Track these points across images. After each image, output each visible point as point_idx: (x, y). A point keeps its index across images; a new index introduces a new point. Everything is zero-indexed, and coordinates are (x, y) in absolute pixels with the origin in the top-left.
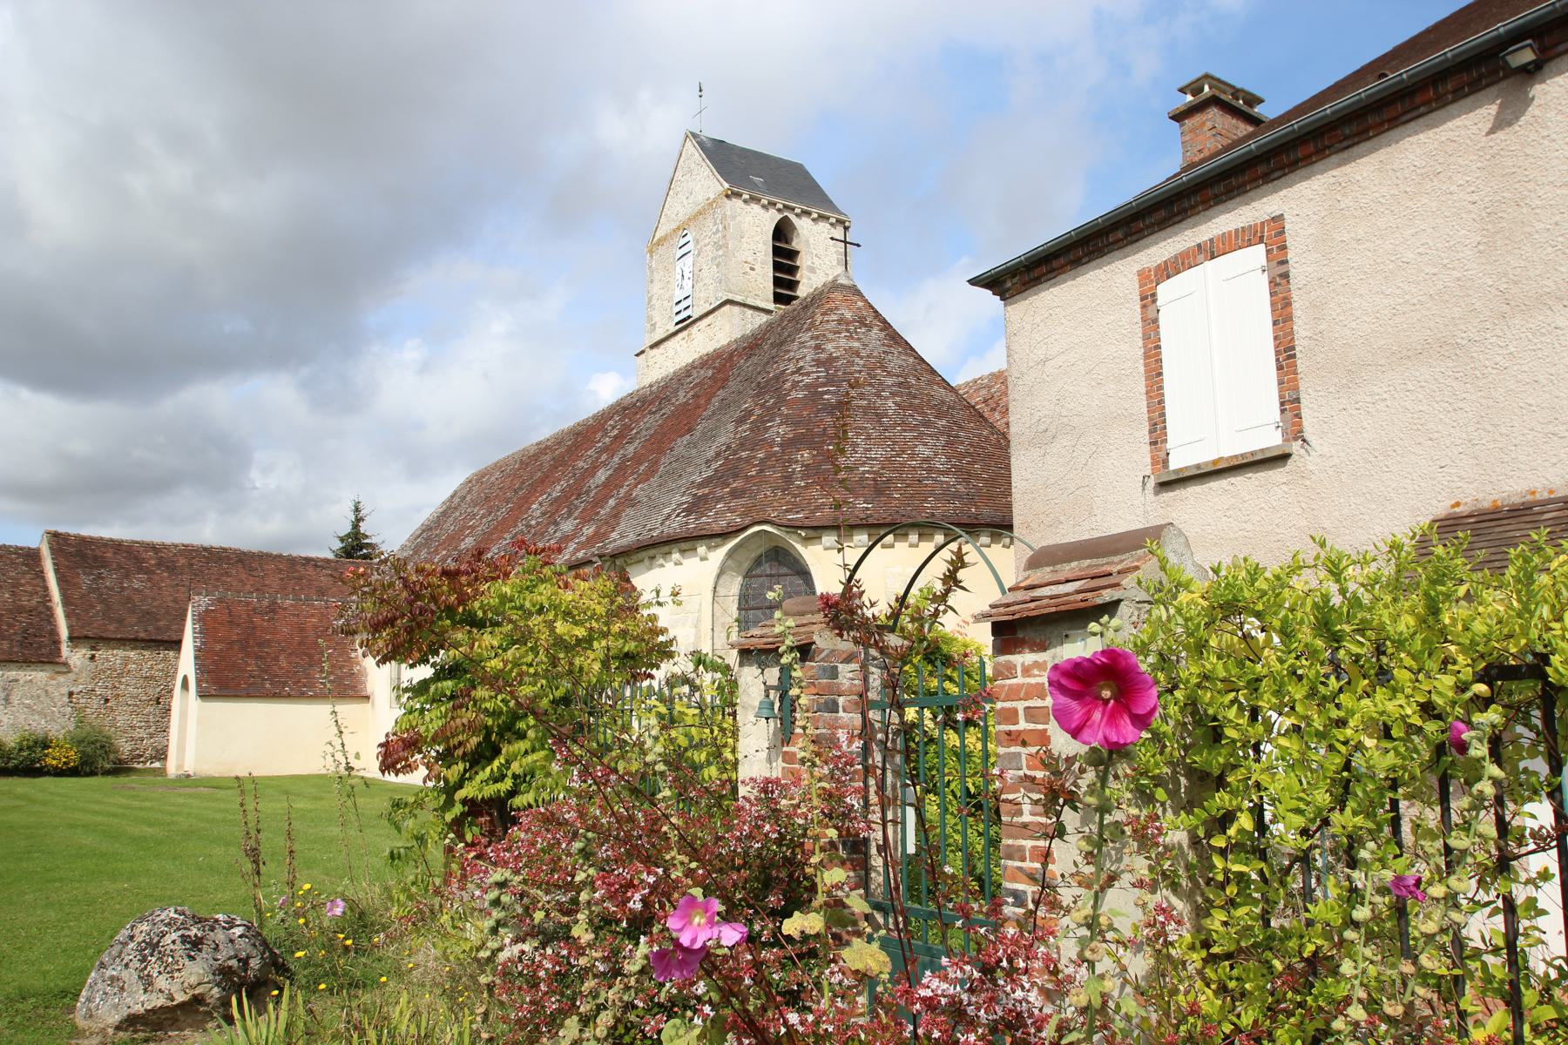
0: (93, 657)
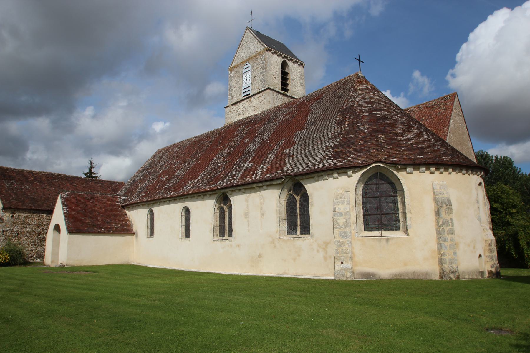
0: (13, 216)
